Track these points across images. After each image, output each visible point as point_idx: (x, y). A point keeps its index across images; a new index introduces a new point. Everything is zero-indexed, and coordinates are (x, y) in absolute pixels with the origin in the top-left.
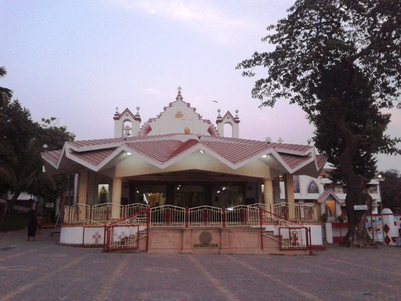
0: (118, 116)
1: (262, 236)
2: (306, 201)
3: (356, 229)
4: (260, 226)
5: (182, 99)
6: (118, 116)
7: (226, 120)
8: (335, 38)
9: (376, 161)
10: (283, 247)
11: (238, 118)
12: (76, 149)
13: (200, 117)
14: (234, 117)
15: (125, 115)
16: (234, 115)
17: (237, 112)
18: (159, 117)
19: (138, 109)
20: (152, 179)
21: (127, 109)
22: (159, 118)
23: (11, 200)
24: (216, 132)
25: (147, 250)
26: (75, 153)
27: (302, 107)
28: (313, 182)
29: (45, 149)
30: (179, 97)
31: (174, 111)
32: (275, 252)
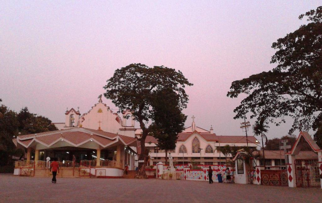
0: (67, 113)
1: (74, 171)
2: (205, 158)
3: (139, 170)
5: (102, 102)
6: (67, 113)
8: (133, 88)
10: (80, 175)
12: (21, 139)
15: (71, 112)
18: (89, 112)
19: (78, 108)
20: (60, 149)
22: (89, 113)
24: (120, 119)
25: (34, 176)
26: (21, 141)
28: (209, 146)
29: (20, 134)
31: (96, 109)
32: (77, 177)
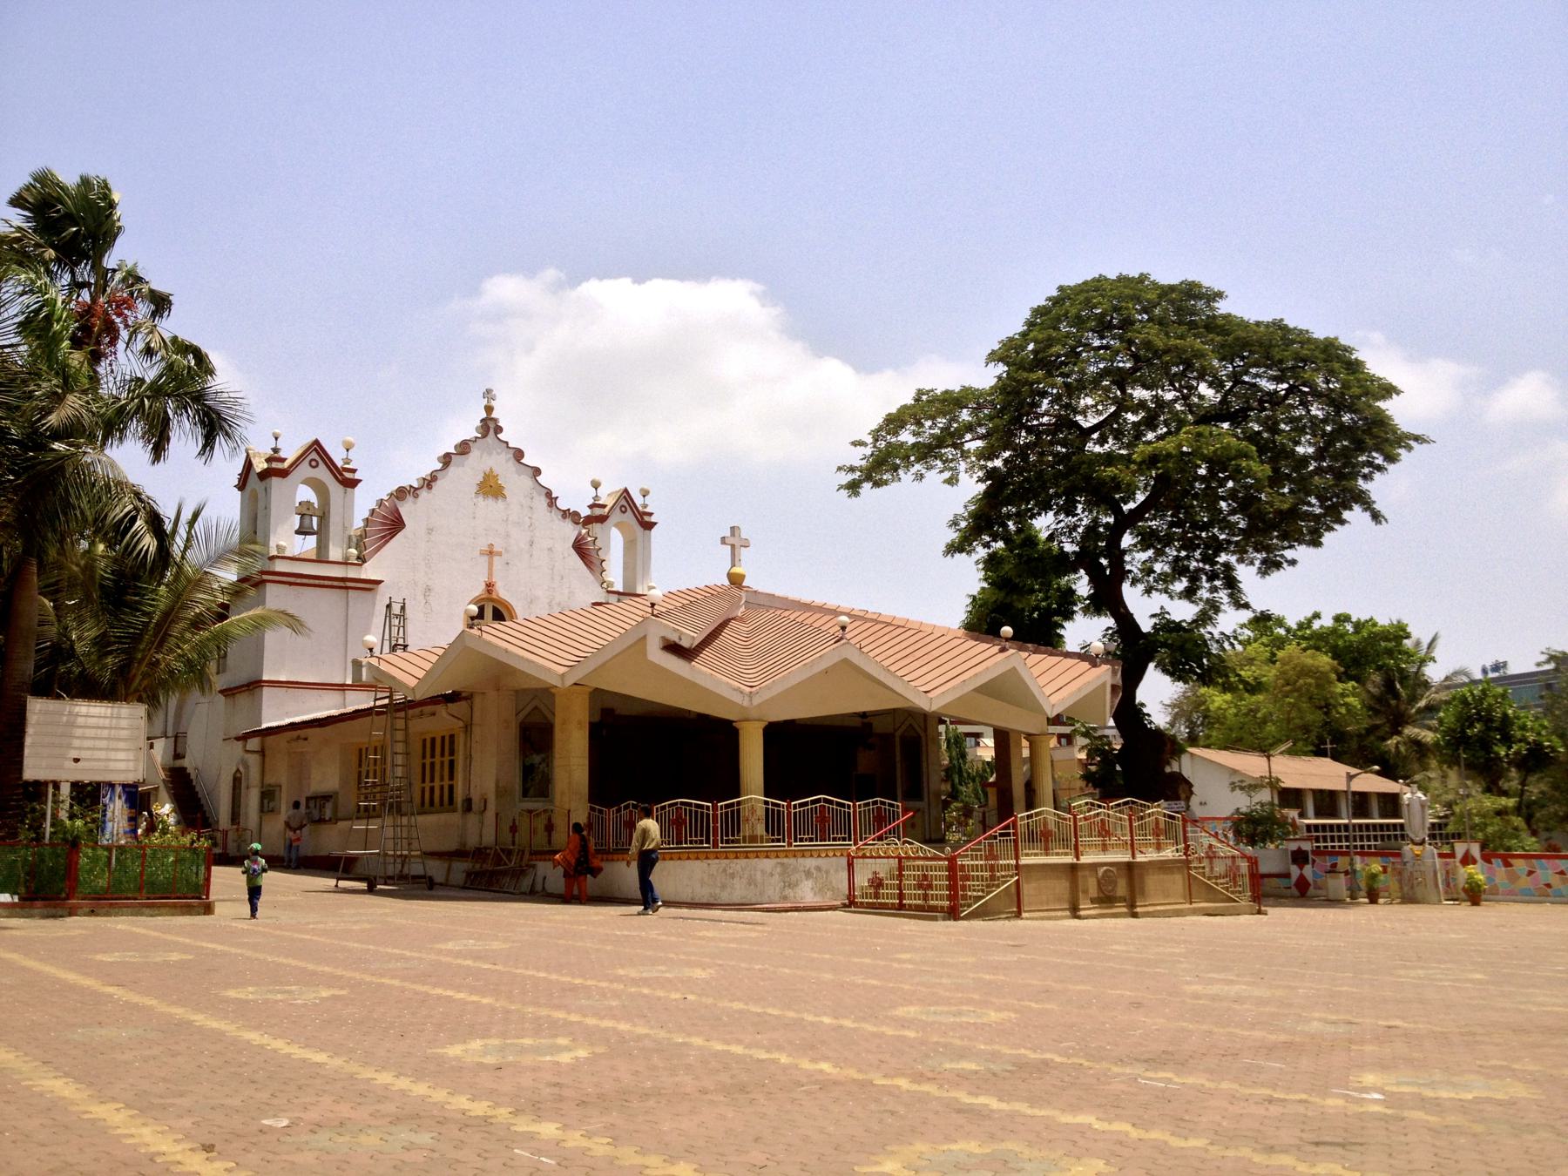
4: (1013, 862)
7: (617, 516)
9: (1293, 562)
11: (650, 514)
13: (551, 500)
14: (339, 464)
15: (306, 462)
16: (639, 500)
17: (645, 493)
21: (317, 442)
23: (1113, 616)
27: (1354, 619)
30: (492, 425)
